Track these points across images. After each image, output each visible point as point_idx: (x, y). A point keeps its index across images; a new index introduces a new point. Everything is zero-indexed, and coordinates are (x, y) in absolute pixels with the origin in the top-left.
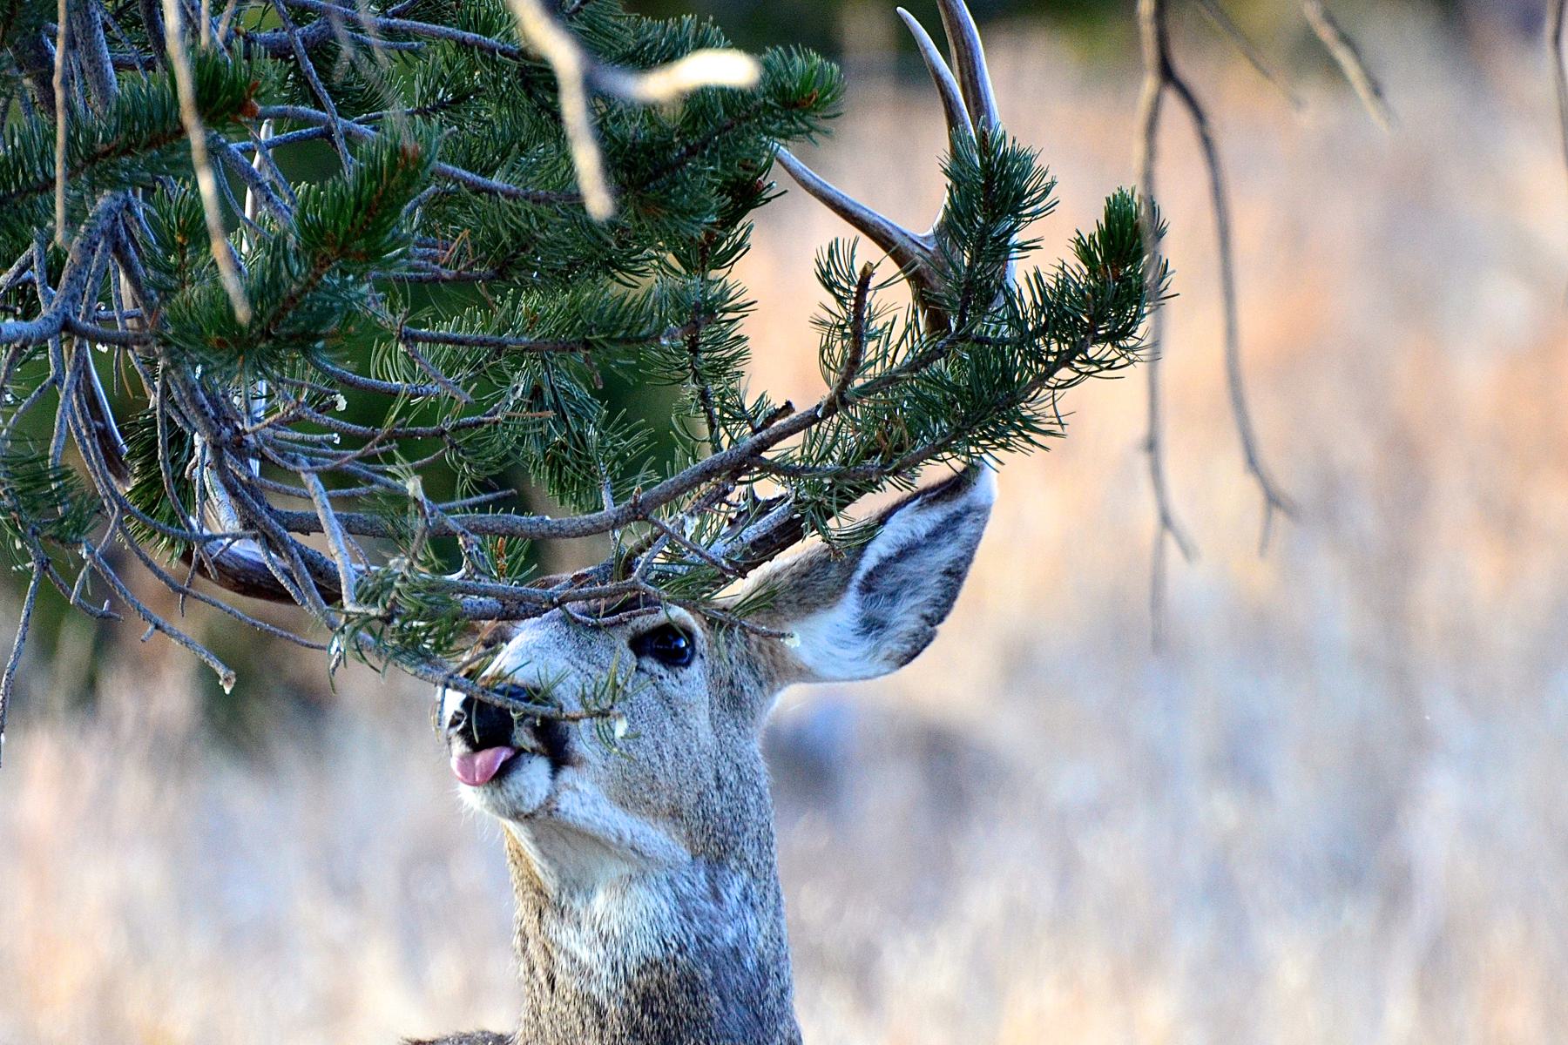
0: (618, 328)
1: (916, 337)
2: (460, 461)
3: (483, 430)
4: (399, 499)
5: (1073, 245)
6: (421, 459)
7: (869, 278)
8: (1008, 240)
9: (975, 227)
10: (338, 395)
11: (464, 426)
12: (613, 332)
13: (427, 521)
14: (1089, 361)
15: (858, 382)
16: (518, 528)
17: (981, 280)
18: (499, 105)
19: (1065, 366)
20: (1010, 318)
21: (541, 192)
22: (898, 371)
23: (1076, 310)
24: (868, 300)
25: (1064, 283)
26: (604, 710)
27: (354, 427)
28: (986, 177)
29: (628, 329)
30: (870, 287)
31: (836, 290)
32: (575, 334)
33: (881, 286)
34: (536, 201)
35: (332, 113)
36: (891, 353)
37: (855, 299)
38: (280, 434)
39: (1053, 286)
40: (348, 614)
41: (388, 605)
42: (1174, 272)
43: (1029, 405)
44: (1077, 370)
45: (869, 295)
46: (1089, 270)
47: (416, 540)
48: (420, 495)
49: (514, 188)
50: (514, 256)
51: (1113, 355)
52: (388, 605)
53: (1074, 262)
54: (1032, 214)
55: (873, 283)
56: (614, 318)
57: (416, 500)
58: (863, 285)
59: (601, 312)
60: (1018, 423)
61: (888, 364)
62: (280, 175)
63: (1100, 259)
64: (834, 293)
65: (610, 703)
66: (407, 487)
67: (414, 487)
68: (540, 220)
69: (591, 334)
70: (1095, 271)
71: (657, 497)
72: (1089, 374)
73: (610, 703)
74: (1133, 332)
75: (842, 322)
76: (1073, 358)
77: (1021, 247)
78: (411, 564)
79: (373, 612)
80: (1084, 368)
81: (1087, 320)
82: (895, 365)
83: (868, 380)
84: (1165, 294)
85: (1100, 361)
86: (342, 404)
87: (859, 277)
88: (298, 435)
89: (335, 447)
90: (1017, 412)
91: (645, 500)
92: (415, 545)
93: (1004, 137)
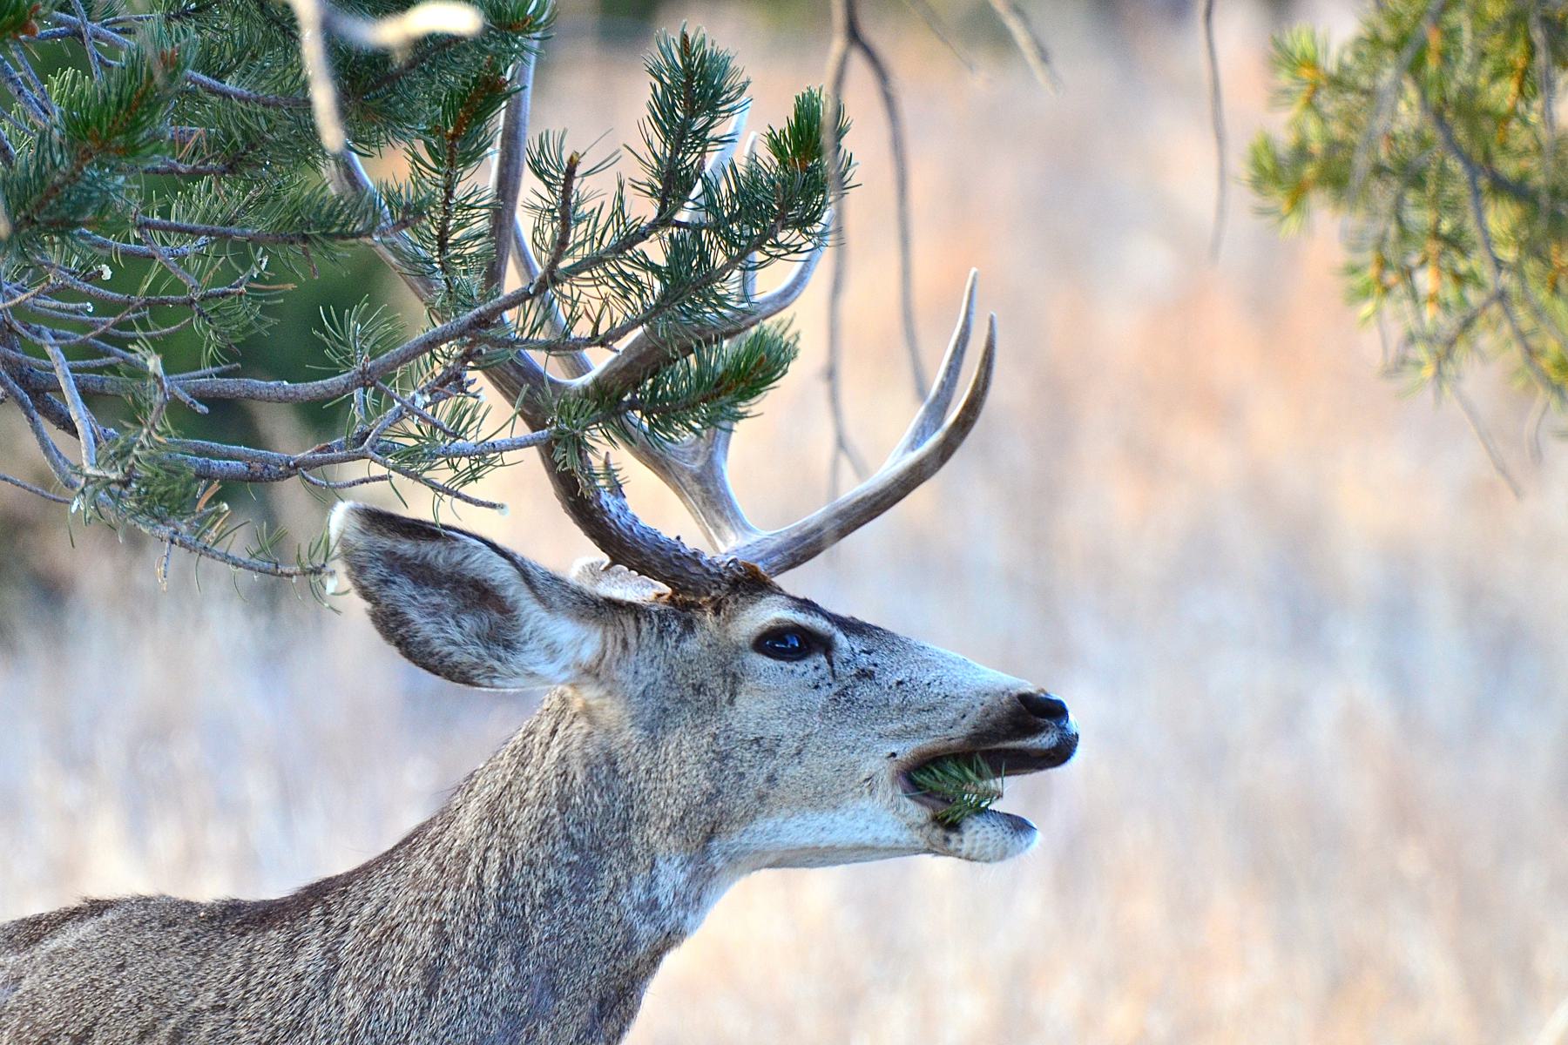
0: (334, 224)
1: (621, 221)
2: (207, 328)
3: (228, 300)
4: (139, 373)
5: (766, 139)
6: (169, 327)
7: (575, 166)
8: (706, 134)
9: (675, 121)
10: (104, 266)
11: (211, 296)
12: (329, 228)
13: (165, 395)
14: (778, 245)
15: (563, 265)
16: (257, 392)
17: (682, 169)
18: (234, 15)
19: (757, 249)
20: (707, 205)
21: (270, 97)
22: (606, 252)
23: (766, 198)
24: (575, 187)
25: (754, 173)
26: (317, 568)
27: (111, 294)
28: (687, 76)
29: (343, 225)
30: (577, 174)
31: (547, 178)
32: (296, 228)
33: (587, 174)
34: (266, 105)
35: (82, 18)
36: (598, 236)
37: (563, 185)
38: (39, 302)
39: (744, 174)
40: (87, 477)
41: (126, 469)
42: (857, 164)
43: (723, 285)
44: (768, 254)
45: (576, 183)
46: (780, 162)
47: (154, 412)
48: (160, 372)
49: (247, 93)
50: (245, 153)
51: (801, 240)
52: (126, 469)
53: (765, 155)
54: (730, 110)
55: (579, 171)
56: (331, 215)
57: (155, 376)
58: (570, 173)
59: (320, 208)
60: (714, 301)
61: (596, 245)
62: (32, 73)
63: (789, 152)
64: (544, 180)
65: (322, 562)
66: (148, 363)
67: (154, 364)
68: (269, 121)
69: (309, 229)
70: (785, 163)
71: (384, 365)
72: (778, 257)
73: (322, 562)
74: (819, 219)
75: (552, 207)
76: (764, 242)
77: (718, 141)
78: (150, 433)
79: (113, 476)
80: (774, 251)
81: (777, 208)
82: (602, 248)
83: (577, 261)
84: (847, 185)
85: (788, 245)
86: (107, 274)
87: (566, 165)
88: (55, 303)
89: (89, 314)
90: (712, 291)
91: (373, 367)
92: (153, 416)
93: (703, 41)
